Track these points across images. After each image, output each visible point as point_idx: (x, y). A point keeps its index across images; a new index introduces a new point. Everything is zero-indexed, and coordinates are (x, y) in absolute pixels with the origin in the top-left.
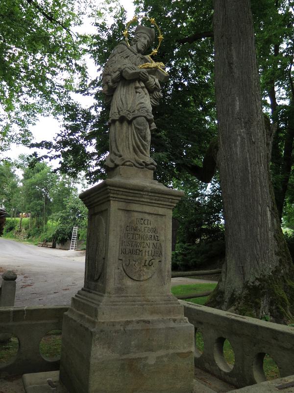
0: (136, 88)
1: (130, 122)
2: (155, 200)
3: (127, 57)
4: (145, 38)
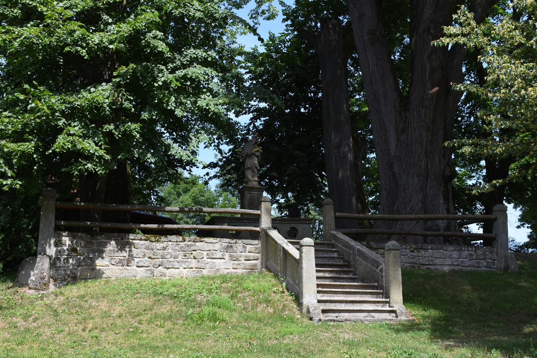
1: (250, 168)
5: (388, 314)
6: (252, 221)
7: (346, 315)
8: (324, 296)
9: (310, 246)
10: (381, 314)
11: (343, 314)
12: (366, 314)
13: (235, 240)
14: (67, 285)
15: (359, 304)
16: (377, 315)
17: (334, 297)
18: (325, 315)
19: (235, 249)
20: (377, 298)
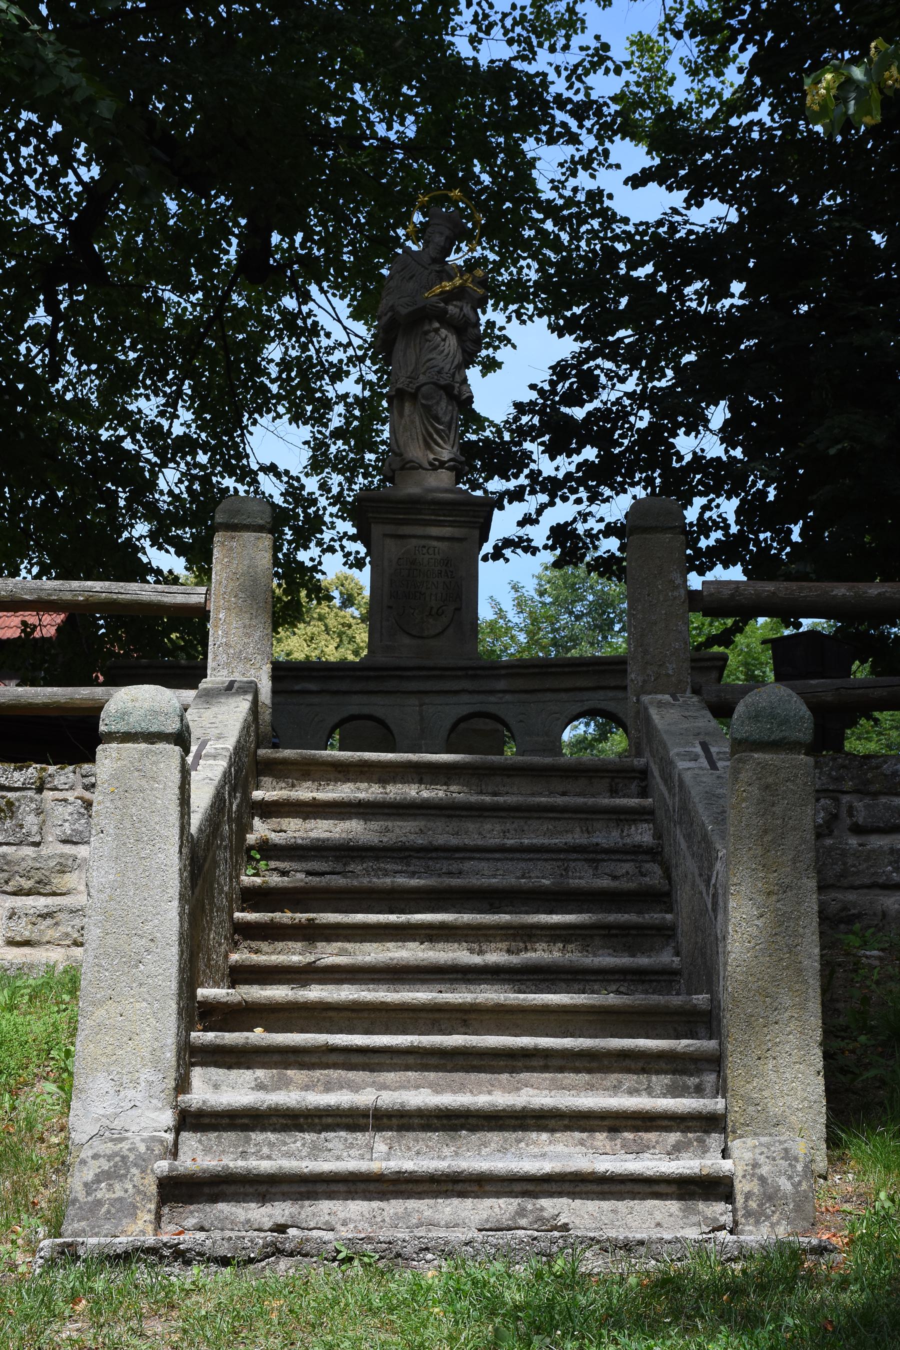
0: (426, 333)
1: (414, 397)
2: (444, 516)
3: (411, 278)
4: (441, 234)
5: (674, 1206)
6: (344, 686)
7: (352, 1216)
8: (285, 1084)
9: (152, 737)
10: (622, 1206)
11: (325, 1206)
12: (500, 1208)
13: (32, 771)
14: (71, 1074)
15: (495, 1138)
16: (582, 1215)
17: (355, 1088)
18: (193, 1214)
19: (31, 821)
20: (674, 1091)
